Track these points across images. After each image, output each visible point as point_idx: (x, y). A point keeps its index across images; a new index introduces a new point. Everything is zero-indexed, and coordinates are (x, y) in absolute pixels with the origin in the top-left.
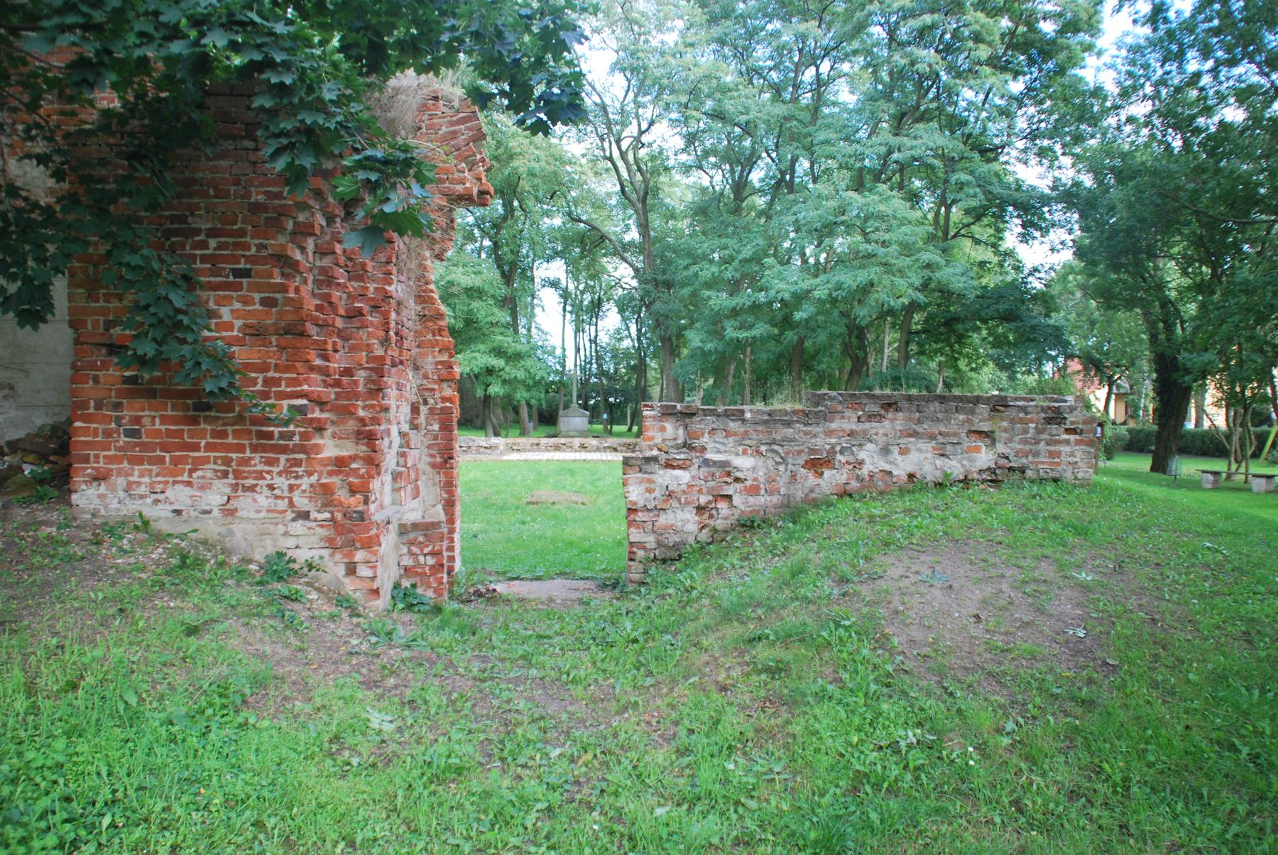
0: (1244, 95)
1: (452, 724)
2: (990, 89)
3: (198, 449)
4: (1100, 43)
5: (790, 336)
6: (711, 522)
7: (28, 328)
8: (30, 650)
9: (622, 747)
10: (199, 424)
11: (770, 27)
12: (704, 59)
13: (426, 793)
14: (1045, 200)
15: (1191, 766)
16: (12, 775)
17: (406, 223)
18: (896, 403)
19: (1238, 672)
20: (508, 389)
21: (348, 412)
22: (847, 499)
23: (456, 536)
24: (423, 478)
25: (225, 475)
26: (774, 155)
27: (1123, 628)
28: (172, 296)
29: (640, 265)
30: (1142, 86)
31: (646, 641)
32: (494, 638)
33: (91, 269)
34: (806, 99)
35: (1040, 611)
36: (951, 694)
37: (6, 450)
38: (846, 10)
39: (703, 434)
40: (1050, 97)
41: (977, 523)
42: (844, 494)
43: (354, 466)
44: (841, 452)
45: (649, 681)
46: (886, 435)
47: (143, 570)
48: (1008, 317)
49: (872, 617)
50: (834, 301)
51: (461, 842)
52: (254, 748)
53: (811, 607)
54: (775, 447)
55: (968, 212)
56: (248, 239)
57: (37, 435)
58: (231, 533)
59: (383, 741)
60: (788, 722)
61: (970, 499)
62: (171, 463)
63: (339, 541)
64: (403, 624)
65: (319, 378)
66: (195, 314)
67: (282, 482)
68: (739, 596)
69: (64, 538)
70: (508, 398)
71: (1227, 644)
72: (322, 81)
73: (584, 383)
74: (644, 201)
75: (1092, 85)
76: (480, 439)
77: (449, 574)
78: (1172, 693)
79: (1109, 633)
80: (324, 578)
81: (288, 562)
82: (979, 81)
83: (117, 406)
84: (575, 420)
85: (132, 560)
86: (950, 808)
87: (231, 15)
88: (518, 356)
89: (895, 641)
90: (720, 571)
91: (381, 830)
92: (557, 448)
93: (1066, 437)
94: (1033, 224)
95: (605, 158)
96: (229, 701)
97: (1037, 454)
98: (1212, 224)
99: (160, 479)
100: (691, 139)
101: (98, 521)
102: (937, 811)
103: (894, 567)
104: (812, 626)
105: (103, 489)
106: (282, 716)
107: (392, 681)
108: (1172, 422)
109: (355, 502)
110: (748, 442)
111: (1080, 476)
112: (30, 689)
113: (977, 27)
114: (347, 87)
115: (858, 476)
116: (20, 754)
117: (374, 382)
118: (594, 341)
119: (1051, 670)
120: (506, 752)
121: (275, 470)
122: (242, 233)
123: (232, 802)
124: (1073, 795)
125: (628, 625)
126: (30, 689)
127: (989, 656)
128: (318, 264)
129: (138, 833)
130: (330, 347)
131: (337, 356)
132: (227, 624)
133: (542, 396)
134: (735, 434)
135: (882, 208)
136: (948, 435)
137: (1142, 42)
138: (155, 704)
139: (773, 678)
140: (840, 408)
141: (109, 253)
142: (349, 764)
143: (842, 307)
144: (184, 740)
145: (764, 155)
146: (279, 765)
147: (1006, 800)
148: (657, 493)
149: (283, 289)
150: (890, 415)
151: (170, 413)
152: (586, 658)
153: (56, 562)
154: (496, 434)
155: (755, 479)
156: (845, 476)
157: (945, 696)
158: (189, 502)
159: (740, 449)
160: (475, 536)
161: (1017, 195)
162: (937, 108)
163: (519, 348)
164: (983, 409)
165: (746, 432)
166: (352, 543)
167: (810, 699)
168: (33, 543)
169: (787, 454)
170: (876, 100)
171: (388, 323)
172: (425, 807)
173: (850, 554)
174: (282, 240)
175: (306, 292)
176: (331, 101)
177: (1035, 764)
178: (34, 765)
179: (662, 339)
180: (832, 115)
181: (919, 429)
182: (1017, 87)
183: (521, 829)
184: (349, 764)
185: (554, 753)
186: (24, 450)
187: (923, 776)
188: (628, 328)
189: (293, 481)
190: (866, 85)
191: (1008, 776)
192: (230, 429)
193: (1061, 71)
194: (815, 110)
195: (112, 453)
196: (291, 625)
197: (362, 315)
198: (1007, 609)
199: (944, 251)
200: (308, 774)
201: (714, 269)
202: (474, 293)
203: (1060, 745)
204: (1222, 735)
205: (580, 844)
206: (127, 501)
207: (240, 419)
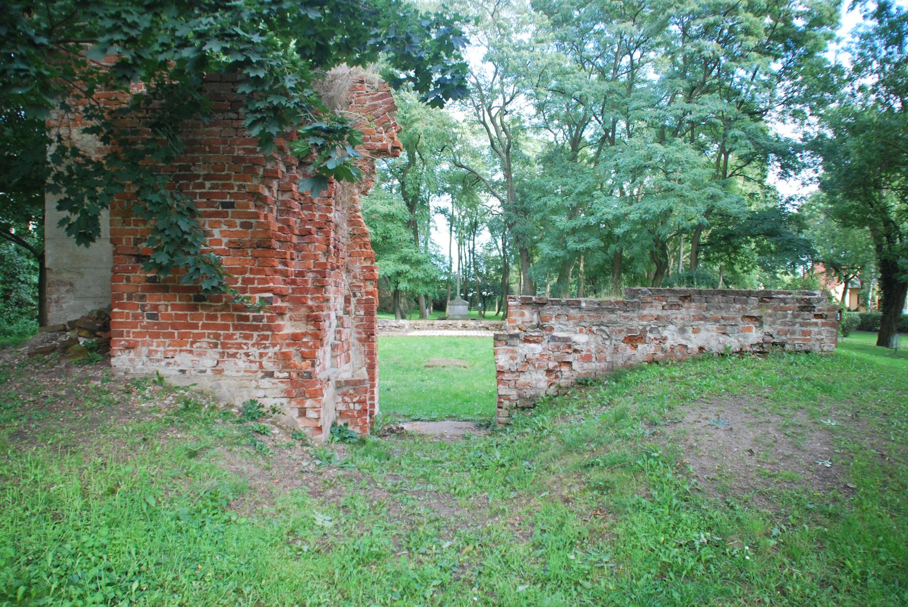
1: (373, 523)
2: (757, 69)
4: (838, 33)
5: (613, 247)
6: (557, 381)
7: (83, 245)
9: (494, 542)
10: (197, 310)
11: (596, 27)
13: (355, 572)
14: (798, 148)
16: (73, 552)
17: (342, 173)
18: (690, 296)
21: (300, 302)
22: (655, 364)
23: (376, 390)
24: (353, 348)
25: (216, 345)
28: (180, 223)
30: (870, 64)
31: (511, 466)
32: (402, 463)
34: (623, 78)
35: (797, 448)
36: (732, 507)
37: (68, 327)
39: (551, 318)
40: (802, 73)
41: (749, 383)
42: (653, 361)
43: (305, 340)
44: (651, 331)
47: (159, 411)
48: (770, 234)
49: (673, 451)
52: (235, 537)
53: (630, 443)
54: (603, 328)
56: (232, 181)
57: (88, 317)
58: (220, 386)
59: (325, 534)
60: (613, 526)
61: (745, 365)
64: (339, 451)
65: (281, 278)
67: (254, 351)
69: (106, 389)
72: (285, 74)
77: (370, 416)
78: (898, 510)
79: (848, 465)
80: (284, 419)
81: (259, 407)
82: (748, 63)
83: (142, 298)
84: (457, 307)
85: (152, 405)
88: (418, 262)
89: (691, 468)
92: (446, 327)
93: (815, 320)
94: (789, 167)
96: (218, 503)
97: (793, 333)
100: (540, 107)
101: (129, 377)
102: (722, 593)
103: (689, 415)
104: (630, 457)
105: (132, 355)
106: (254, 515)
109: (305, 365)
110: (583, 324)
111: (825, 349)
112: (84, 493)
113: (747, 24)
114: (302, 78)
115: (662, 349)
116: (78, 537)
117: (319, 281)
118: (472, 252)
120: (411, 543)
121: (250, 342)
122: (228, 177)
123: (220, 575)
124: (823, 584)
125: (498, 454)
126: (84, 493)
128: (280, 198)
130: (288, 256)
131: (293, 262)
132: (216, 450)
134: (574, 318)
135: (678, 155)
138: (167, 505)
139: (602, 494)
140: (649, 299)
141: (138, 193)
142: (301, 550)
144: (187, 531)
145: (593, 118)
146: (252, 549)
147: (773, 586)
148: (518, 360)
149: (257, 216)
150: (686, 305)
151: (178, 302)
153: (101, 405)
154: (403, 317)
155: (589, 351)
156: (653, 348)
157: (728, 509)
158: (190, 364)
159: (578, 329)
160: (389, 390)
162: (718, 83)
163: (420, 256)
164: (754, 300)
165: (582, 317)
167: (629, 509)
168: (86, 392)
169: (612, 332)
170: (674, 78)
171: (329, 240)
174: (255, 182)
175: (272, 218)
176: (291, 88)
177: (795, 560)
178: (87, 545)
179: (521, 250)
180: (642, 89)
181: (707, 315)
182: (776, 66)
183: (422, 599)
184: (301, 550)
186: (79, 328)
187: (712, 566)
188: (496, 242)
189: (262, 351)
190: (667, 67)
191: (775, 568)
192: (219, 314)
193: (810, 54)
194: (630, 85)
195: (139, 330)
196: (260, 451)
198: (773, 446)
201: (558, 199)
202: (389, 217)
206: (149, 363)
207: (226, 307)
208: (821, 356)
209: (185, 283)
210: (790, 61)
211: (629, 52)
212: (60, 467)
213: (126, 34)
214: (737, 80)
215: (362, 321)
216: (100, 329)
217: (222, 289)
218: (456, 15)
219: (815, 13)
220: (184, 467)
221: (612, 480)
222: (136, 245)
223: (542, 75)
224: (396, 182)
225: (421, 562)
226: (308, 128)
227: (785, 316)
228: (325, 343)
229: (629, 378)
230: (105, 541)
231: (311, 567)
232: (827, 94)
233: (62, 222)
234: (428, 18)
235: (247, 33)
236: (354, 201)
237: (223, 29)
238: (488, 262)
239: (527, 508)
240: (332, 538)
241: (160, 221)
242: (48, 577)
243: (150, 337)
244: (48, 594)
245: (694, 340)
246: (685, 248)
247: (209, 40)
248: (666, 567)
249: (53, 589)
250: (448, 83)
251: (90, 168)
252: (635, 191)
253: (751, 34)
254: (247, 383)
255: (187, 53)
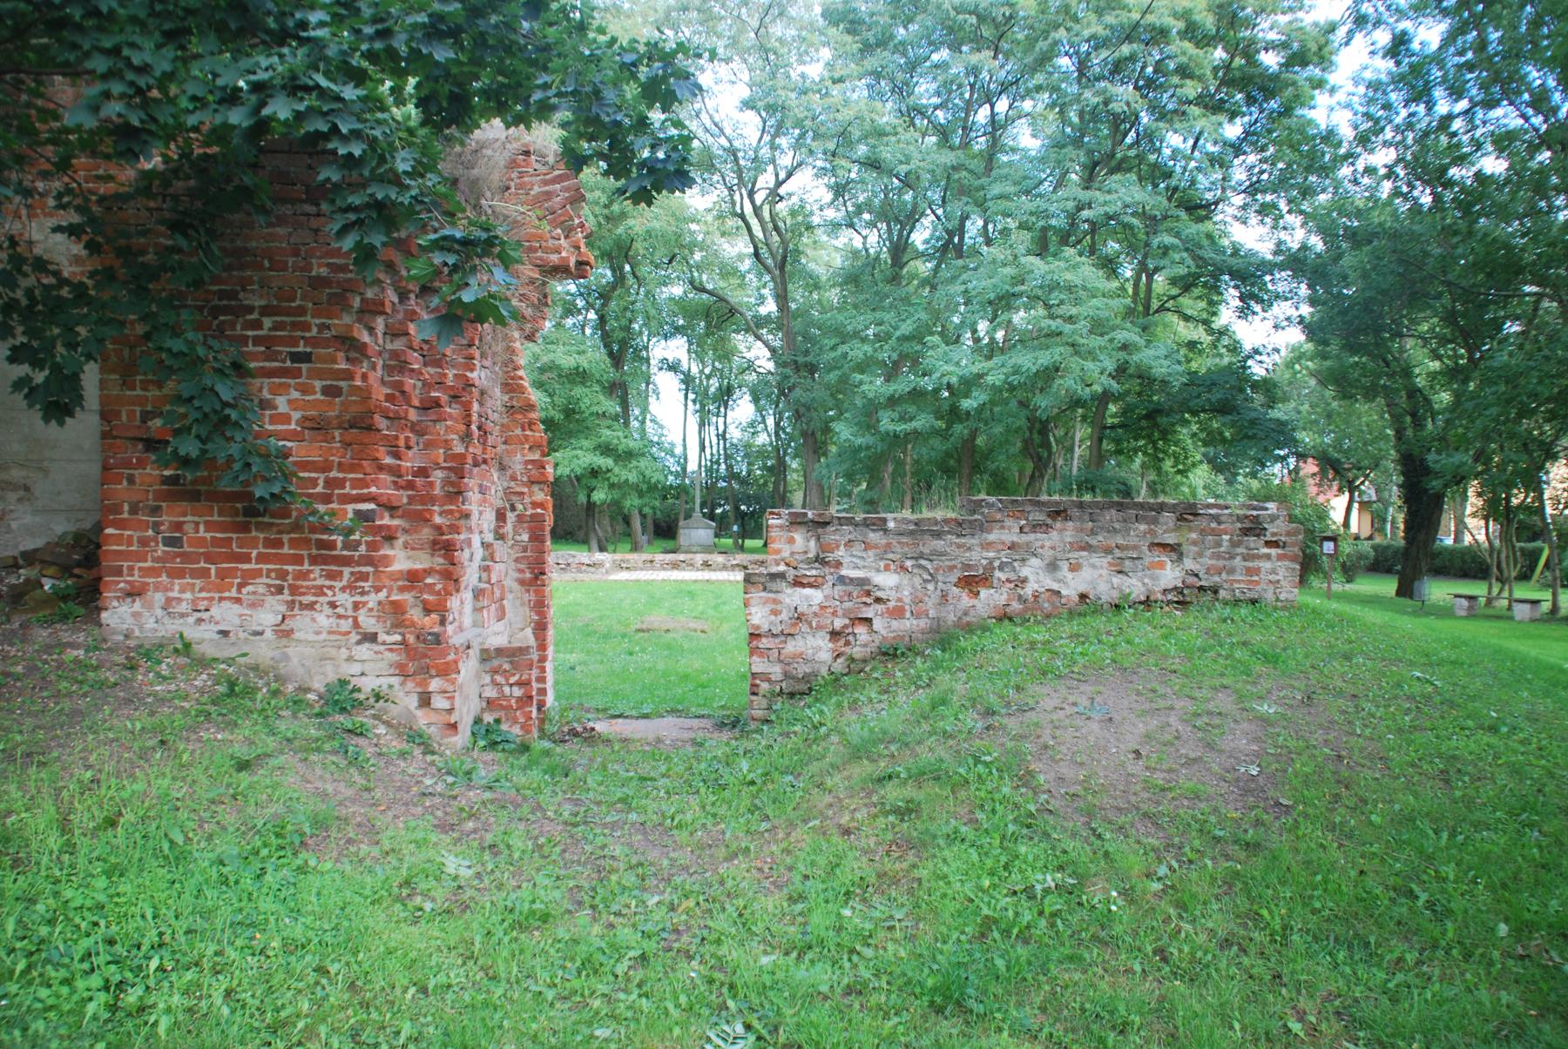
0: (1504, 141)
1: (538, 870)
2: (1201, 133)
3: (249, 561)
4: (1332, 78)
5: (958, 429)
6: (848, 650)
7: (54, 422)
8: (61, 784)
9: (729, 895)
10: (249, 531)
11: (935, 57)
12: (855, 96)
13: (506, 940)
14: (1268, 267)
15: (1361, 913)
16: (48, 916)
17: (483, 311)
18: (1065, 511)
19: (1428, 814)
20: (616, 494)
21: (422, 518)
22: (1006, 622)
23: (549, 666)
24: (510, 596)
25: (280, 590)
26: (940, 212)
27: (1303, 765)
28: (219, 388)
29: (777, 344)
30: (1382, 129)
31: (764, 783)
32: (589, 780)
33: (126, 352)
34: (981, 144)
35: (1210, 746)
36: (1099, 837)
37: (21, 562)
38: (1027, 37)
39: (838, 547)
40: (1274, 142)
41: (1152, 649)
42: (1004, 617)
43: (429, 581)
44: (1001, 568)
45: (764, 826)
46: (1053, 548)
47: (185, 698)
48: (1223, 408)
49: (1017, 753)
50: (1012, 388)
51: (544, 990)
52: (314, 891)
53: (951, 742)
54: (923, 562)
55: (1173, 281)
56: (309, 318)
57: (57, 544)
58: (286, 657)
59: (460, 887)
60: (914, 866)
61: (1149, 622)
62: (217, 576)
63: (411, 668)
64: (485, 763)
65: (389, 478)
66: (245, 408)
67: (345, 599)
68: (871, 731)
69: (94, 662)
70: (616, 504)
71: (1420, 783)
72: (396, 149)
73: (709, 489)
74: (782, 266)
75: (1323, 127)
76: (581, 555)
77: (539, 709)
78: (1350, 836)
79: (1285, 771)
80: (394, 710)
81: (352, 691)
82: (1185, 125)
83: (156, 511)
84: (697, 532)
85: (173, 687)
86: (1087, 956)
87: (294, 78)
88: (630, 455)
89: (1042, 778)
90: (854, 706)
91: (456, 976)
92: (675, 566)
93: (1266, 550)
94: (1254, 296)
95: (735, 214)
96: (289, 841)
97: (1232, 571)
98: (1468, 295)
99: (204, 595)
100: (839, 190)
101: (132, 643)
102: (1071, 958)
103: (1047, 698)
104: (949, 763)
105: (137, 606)
106: (346, 860)
107: (471, 825)
108: (1421, 537)
109: (429, 622)
110: (891, 556)
111: (1282, 597)
112: (64, 826)
113: (1184, 59)
114: (424, 155)
115: (1020, 596)
116: (56, 894)
117: (452, 484)
118: (722, 436)
119: (1215, 810)
120: (598, 899)
121: (338, 585)
122: (301, 311)
123: (292, 947)
124: (1226, 943)
125: (745, 765)
126: (64, 826)
127: (1146, 795)
128: (389, 346)
129: (189, 976)
130: (402, 443)
131: (410, 453)
132: (283, 758)
133: (657, 503)
134: (876, 547)
135: (1068, 276)
136: (1127, 548)
137: (1383, 77)
138: (203, 844)
139: (902, 820)
140: (999, 516)
141: (147, 336)
142: (421, 909)
143: (1021, 394)
144: (237, 882)
145: (928, 211)
146: (342, 909)
147: (1149, 949)
148: (784, 616)
149: (349, 375)
150: (1058, 525)
151: (216, 518)
152: (694, 802)
153: (86, 688)
154: (602, 549)
155: (899, 600)
156: (1005, 596)
157: (1092, 839)
158: (237, 621)
159: (882, 564)
160: (572, 668)
161: (1233, 261)
162: (1137, 156)
163: (632, 444)
164: (1168, 518)
165: (889, 545)
166: (425, 670)
167: (941, 842)
168: (58, 668)
169: (937, 569)
170: (1063, 146)
171: (469, 415)
172: (505, 953)
173: (1000, 684)
174: (347, 319)
175: (374, 379)
176: (405, 173)
177: (1186, 911)
178: (73, 905)
179: (804, 434)
180: (1010, 164)
181: (1093, 542)
182: (1233, 131)
183: (611, 978)
184: (421, 909)
185: (653, 901)
186: (43, 562)
187: (1059, 922)
188: (764, 421)
189: (358, 598)
190: (1052, 126)
191: (1155, 923)
192: (285, 538)
193: (1287, 111)
194: (989, 157)
195: (149, 564)
196: (354, 761)
197: (439, 406)
198: (1172, 744)
199: (1144, 329)
200: (376, 919)
201: (867, 348)
202: (579, 376)
203: (1216, 891)
204: (1399, 881)
205: (675, 992)
206: (166, 620)
207: (296, 527)
208: (1275, 608)
209: (225, 485)
210: (1256, 121)
211: (989, 99)
212: (22, 787)
213: (132, 84)
214: (1167, 152)
215: (525, 550)
216: (79, 564)
217: (288, 499)
218: (680, 45)
219: (1296, 45)
220: (229, 786)
221: (917, 799)
222: (144, 422)
223: (843, 134)
224: (592, 315)
225: (611, 926)
226: (433, 236)
227: (1219, 544)
228: (462, 586)
229: (963, 643)
230: (102, 898)
231: (436, 934)
232: (1313, 178)
233: (18, 385)
234: (634, 50)
235: (334, 81)
236: (513, 352)
237: (294, 78)
238: (750, 453)
239: (785, 844)
240: (469, 893)
241: (184, 384)
242: (9, 955)
243: (169, 576)
244: (11, 979)
245: (1072, 583)
246: (1082, 432)
247: (271, 96)
248: (988, 923)
249: (17, 972)
250: (659, 166)
251: (65, 292)
252: (1000, 335)
253: (1191, 76)
254: (333, 652)
255: (237, 117)
